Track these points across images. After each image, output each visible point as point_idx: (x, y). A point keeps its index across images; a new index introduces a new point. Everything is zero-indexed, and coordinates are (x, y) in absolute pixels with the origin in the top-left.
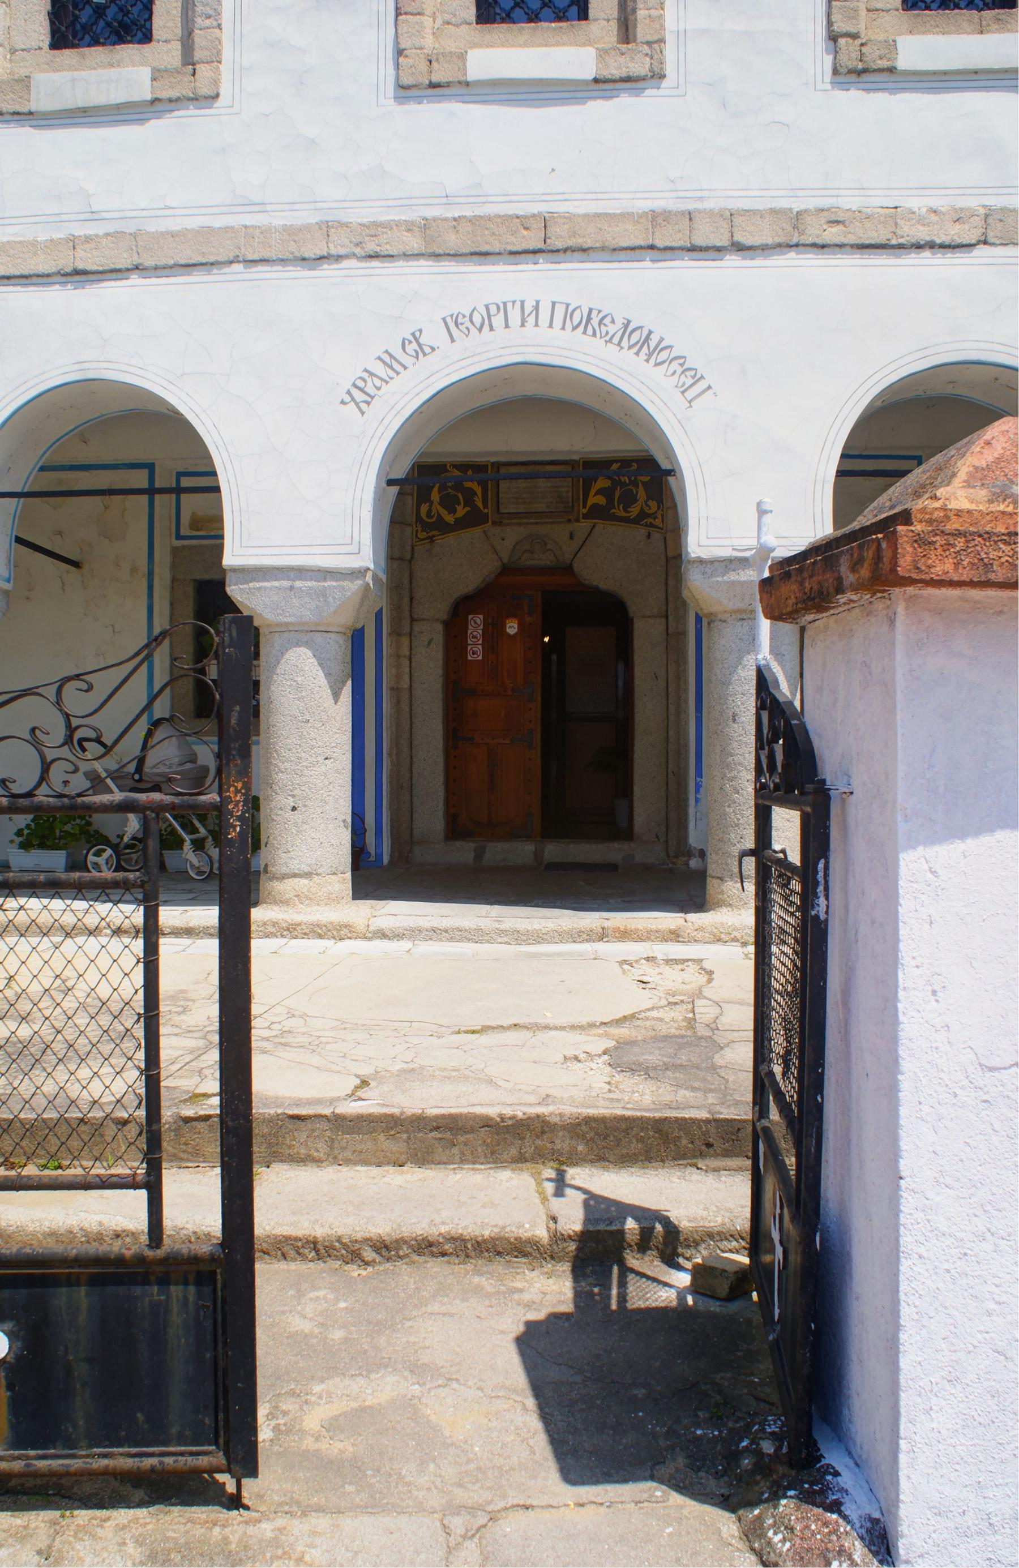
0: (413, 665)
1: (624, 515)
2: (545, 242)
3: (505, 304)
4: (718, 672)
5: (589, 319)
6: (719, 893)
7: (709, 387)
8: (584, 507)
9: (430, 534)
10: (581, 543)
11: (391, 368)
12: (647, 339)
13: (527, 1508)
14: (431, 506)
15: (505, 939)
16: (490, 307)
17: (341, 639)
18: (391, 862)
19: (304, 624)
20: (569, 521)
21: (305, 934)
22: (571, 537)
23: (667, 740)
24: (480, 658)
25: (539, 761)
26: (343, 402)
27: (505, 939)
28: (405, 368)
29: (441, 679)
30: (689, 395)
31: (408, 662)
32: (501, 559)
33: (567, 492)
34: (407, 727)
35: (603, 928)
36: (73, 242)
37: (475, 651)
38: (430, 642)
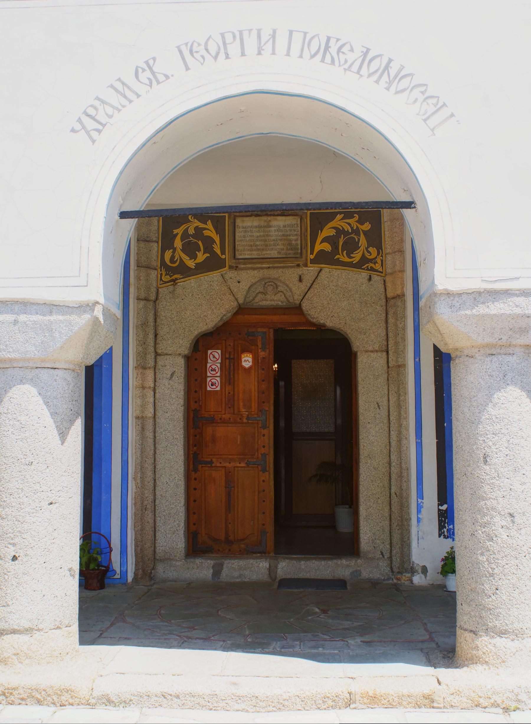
0: (157, 395)
1: (347, 260)
3: (241, 32)
4: (466, 410)
5: (327, 47)
6: (473, 649)
7: (452, 115)
8: (312, 253)
9: (173, 277)
10: (309, 285)
11: (125, 97)
12: (387, 67)
14: (174, 252)
15: (242, 706)
16: (226, 35)
17: (69, 376)
18: (136, 579)
19: (29, 360)
20: (298, 265)
21: (22, 699)
22: (300, 280)
23: (390, 464)
24: (218, 389)
25: (272, 483)
26: (73, 130)
27: (242, 706)
28: (138, 96)
29: (182, 408)
30: (432, 122)
31: (152, 393)
32: (236, 300)
33: (297, 240)
34: (151, 453)
35: (350, 694)
37: (214, 381)
38: (172, 375)
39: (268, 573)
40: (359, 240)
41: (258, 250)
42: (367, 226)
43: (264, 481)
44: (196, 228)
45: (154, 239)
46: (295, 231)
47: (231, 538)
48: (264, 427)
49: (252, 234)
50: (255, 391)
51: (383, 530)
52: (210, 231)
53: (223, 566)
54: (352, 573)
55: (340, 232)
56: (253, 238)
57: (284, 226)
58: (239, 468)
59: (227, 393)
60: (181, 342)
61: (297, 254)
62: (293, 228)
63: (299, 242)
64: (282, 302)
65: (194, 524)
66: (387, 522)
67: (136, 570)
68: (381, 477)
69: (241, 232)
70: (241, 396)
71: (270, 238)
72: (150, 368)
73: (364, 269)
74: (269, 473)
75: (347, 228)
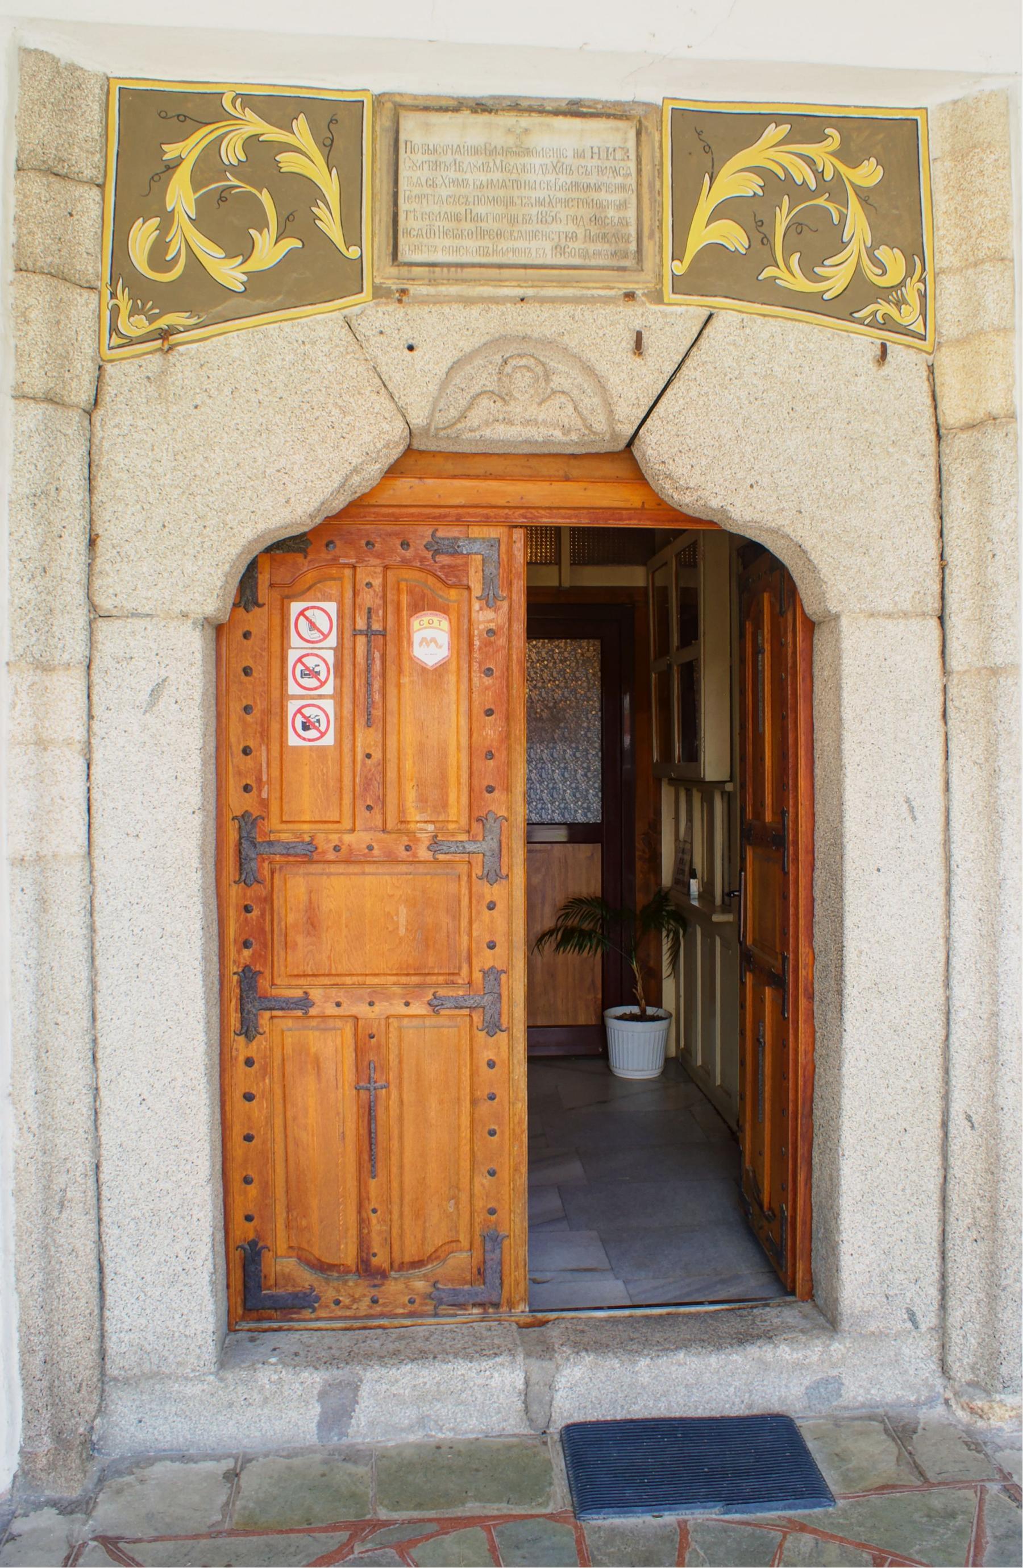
1: (801, 284)
8: (677, 255)
9: (162, 323)
14: (165, 228)
20: (630, 296)
22: (638, 345)
24: (329, 740)
31: (80, 763)
33: (623, 205)
38: (156, 693)
39: (520, 1406)
40: (843, 218)
41: (483, 234)
42: (868, 174)
43: (491, 1064)
44: (252, 143)
45: (88, 173)
46: (615, 171)
47: (380, 1260)
48: (493, 876)
49: (459, 176)
50: (458, 749)
51: (918, 1239)
52: (304, 158)
53: (357, 1388)
54: (812, 1390)
55: (776, 185)
56: (463, 191)
57: (580, 155)
58: (406, 1021)
59: (360, 756)
60: (189, 568)
61: (625, 256)
62: (614, 164)
63: (631, 214)
64: (566, 430)
65: (249, 1218)
66: (933, 1212)
67: (28, 1439)
68: (914, 1058)
69: (421, 167)
70: (408, 765)
71: (524, 193)
72: (68, 666)
73: (861, 322)
74: (511, 1037)
75: (802, 173)
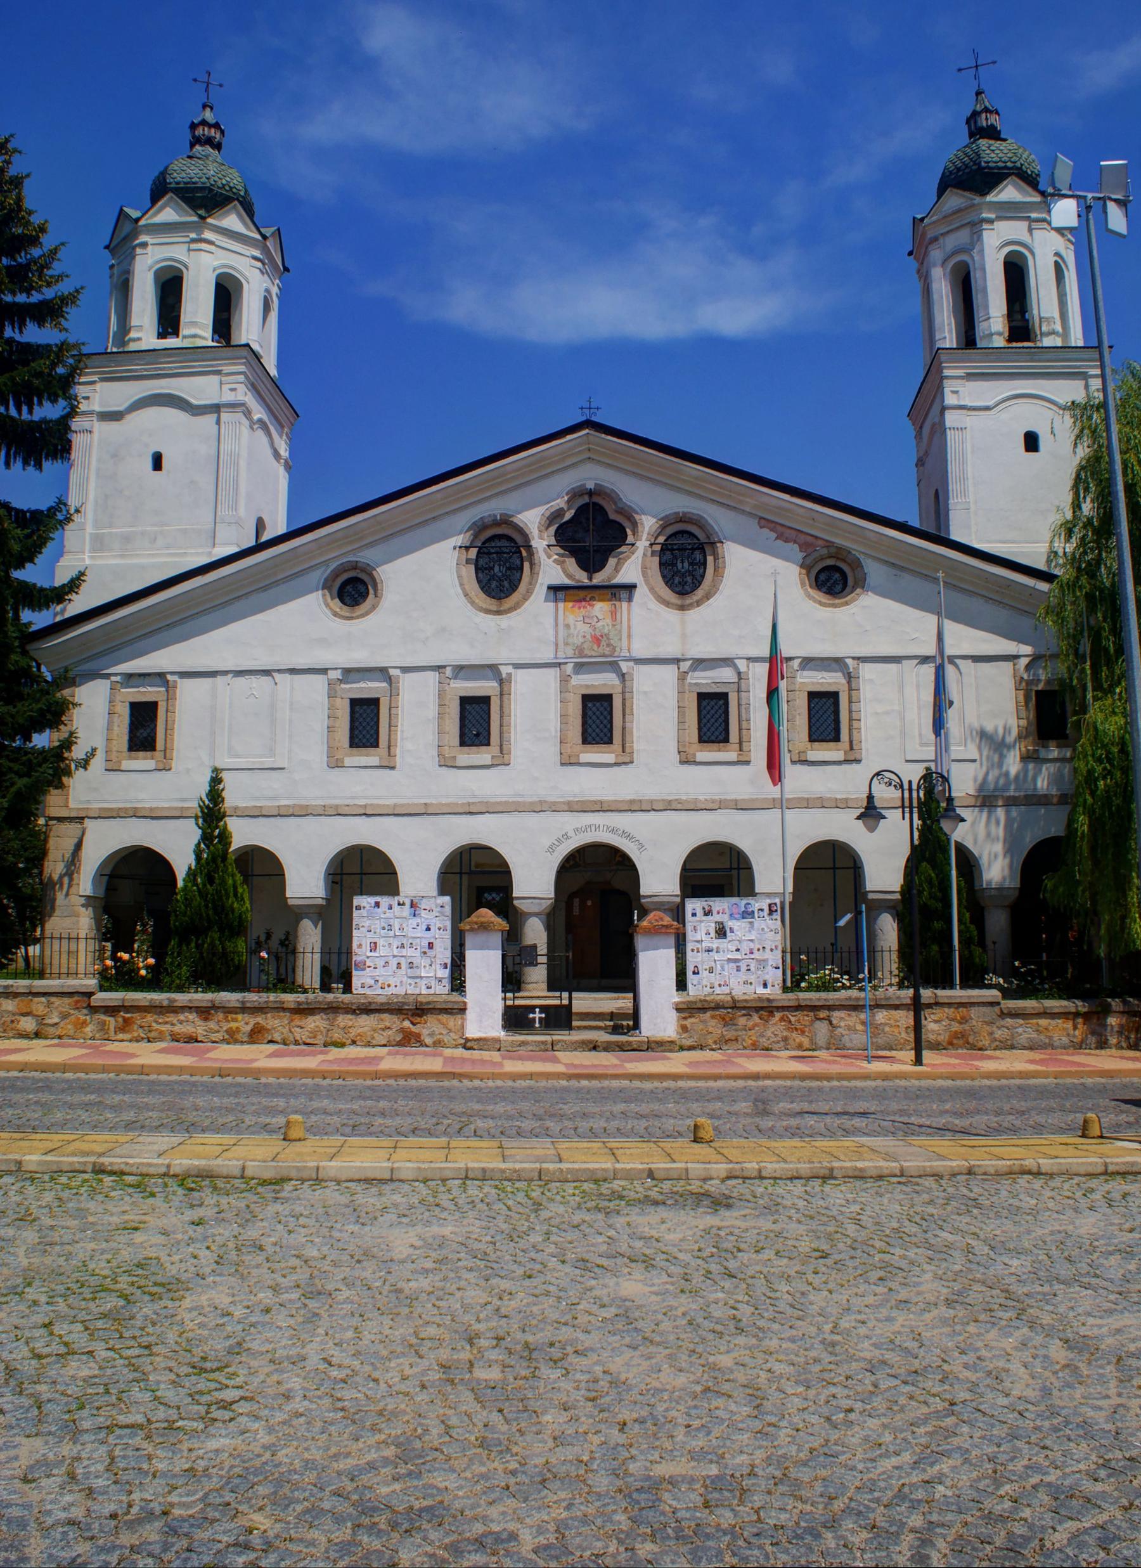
2: (601, 807)
13: (623, 675)
36: (469, 804)
